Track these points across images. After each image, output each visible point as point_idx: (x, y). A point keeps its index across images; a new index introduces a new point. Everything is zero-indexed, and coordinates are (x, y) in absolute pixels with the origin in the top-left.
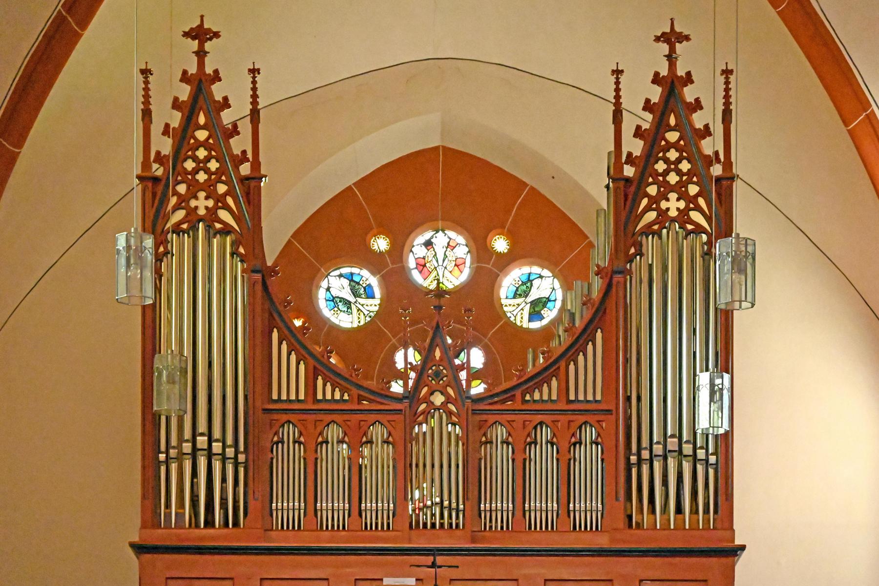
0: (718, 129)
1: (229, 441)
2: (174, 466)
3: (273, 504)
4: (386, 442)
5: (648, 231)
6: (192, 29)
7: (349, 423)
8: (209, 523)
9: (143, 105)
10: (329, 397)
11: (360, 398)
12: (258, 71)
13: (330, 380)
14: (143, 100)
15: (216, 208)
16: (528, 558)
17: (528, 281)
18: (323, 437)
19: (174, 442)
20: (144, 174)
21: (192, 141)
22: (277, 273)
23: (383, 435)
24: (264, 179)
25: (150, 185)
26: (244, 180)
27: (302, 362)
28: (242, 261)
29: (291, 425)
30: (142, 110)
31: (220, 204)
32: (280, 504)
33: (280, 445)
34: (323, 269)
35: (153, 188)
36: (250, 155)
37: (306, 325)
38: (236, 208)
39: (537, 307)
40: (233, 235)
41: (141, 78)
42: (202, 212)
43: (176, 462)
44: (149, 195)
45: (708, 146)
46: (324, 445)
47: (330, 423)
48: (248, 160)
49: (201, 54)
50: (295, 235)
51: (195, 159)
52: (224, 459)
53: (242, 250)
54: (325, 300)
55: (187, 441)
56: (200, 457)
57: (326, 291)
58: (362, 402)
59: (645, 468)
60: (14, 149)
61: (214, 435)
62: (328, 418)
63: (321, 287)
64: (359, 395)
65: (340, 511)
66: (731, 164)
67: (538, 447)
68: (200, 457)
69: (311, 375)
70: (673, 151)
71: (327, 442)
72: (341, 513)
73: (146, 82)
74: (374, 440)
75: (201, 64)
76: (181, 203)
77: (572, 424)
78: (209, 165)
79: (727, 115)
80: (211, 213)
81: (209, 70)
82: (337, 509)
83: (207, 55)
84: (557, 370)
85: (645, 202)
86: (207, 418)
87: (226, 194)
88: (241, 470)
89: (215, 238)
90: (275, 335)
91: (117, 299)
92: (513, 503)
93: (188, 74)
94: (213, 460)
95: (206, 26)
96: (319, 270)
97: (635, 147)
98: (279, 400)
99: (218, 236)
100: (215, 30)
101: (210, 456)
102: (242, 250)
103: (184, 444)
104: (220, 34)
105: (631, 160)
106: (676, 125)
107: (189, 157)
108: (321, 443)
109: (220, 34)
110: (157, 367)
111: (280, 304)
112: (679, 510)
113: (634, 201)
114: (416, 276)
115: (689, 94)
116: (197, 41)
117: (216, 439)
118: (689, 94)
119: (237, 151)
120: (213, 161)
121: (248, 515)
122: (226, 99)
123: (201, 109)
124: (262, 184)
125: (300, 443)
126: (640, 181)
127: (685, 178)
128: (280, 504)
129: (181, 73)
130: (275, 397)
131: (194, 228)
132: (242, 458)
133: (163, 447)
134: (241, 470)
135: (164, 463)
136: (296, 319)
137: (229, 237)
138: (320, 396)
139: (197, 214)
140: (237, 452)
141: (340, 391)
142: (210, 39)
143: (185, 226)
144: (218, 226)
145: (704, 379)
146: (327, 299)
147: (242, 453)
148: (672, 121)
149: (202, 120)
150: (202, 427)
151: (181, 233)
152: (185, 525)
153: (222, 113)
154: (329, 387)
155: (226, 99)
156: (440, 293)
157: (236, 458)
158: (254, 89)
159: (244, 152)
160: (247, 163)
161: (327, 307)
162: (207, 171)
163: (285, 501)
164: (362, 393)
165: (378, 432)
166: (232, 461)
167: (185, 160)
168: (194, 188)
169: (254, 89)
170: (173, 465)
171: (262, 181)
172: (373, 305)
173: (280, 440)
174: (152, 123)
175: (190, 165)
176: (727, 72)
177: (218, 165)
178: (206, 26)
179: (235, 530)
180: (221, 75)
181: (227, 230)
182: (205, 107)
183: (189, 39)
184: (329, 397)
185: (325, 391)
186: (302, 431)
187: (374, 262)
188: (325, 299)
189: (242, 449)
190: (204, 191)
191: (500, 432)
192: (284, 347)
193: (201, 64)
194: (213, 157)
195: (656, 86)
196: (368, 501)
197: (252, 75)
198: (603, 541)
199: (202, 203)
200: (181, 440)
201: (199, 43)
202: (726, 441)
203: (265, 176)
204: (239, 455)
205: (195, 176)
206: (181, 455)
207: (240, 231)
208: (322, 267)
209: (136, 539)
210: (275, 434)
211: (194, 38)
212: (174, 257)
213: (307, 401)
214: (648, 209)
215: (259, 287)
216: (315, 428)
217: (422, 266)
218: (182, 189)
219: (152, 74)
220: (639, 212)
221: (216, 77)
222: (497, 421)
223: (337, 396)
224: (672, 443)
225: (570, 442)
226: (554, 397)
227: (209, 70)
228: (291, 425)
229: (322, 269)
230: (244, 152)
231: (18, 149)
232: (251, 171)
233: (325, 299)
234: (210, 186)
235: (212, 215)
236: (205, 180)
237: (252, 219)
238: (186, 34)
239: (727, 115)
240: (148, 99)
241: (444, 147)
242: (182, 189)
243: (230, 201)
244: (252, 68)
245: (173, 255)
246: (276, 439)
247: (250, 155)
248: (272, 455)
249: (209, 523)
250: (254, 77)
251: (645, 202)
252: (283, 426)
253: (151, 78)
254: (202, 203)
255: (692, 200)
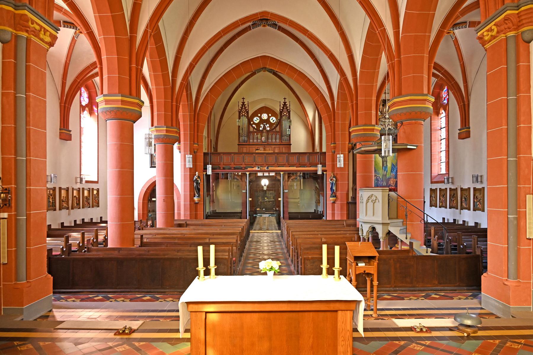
0: (289, 107)
5: (283, 116)
8: (244, 142)
17: (273, 118)
26: (247, 111)
39: (273, 121)
45: (288, 108)
49: (243, 100)
52: (246, 137)
79: (290, 106)
86: (1, 71)
97: (282, 108)
98: (477, 244)
105: (281, 109)
112: (286, 141)
113: (178, 251)
114: (263, 118)
115: (286, 104)
118: (286, 104)
126: (282, 112)
131: (243, 116)
145: (288, 129)
156: (265, 119)
165: (259, 134)
168: (243, 112)
172: (258, 121)
175: (242, 110)
176: (290, 102)
181: (246, 116)
185: (255, 130)
187: (259, 117)
191: (270, 134)
198: (279, 144)
199: (244, 114)
202: (290, 135)
217: (263, 117)
221: (245, 102)
224: (285, 135)
235: (244, 115)
239: (290, 106)
241: (265, 107)
249: (244, 142)
254: (244, 114)
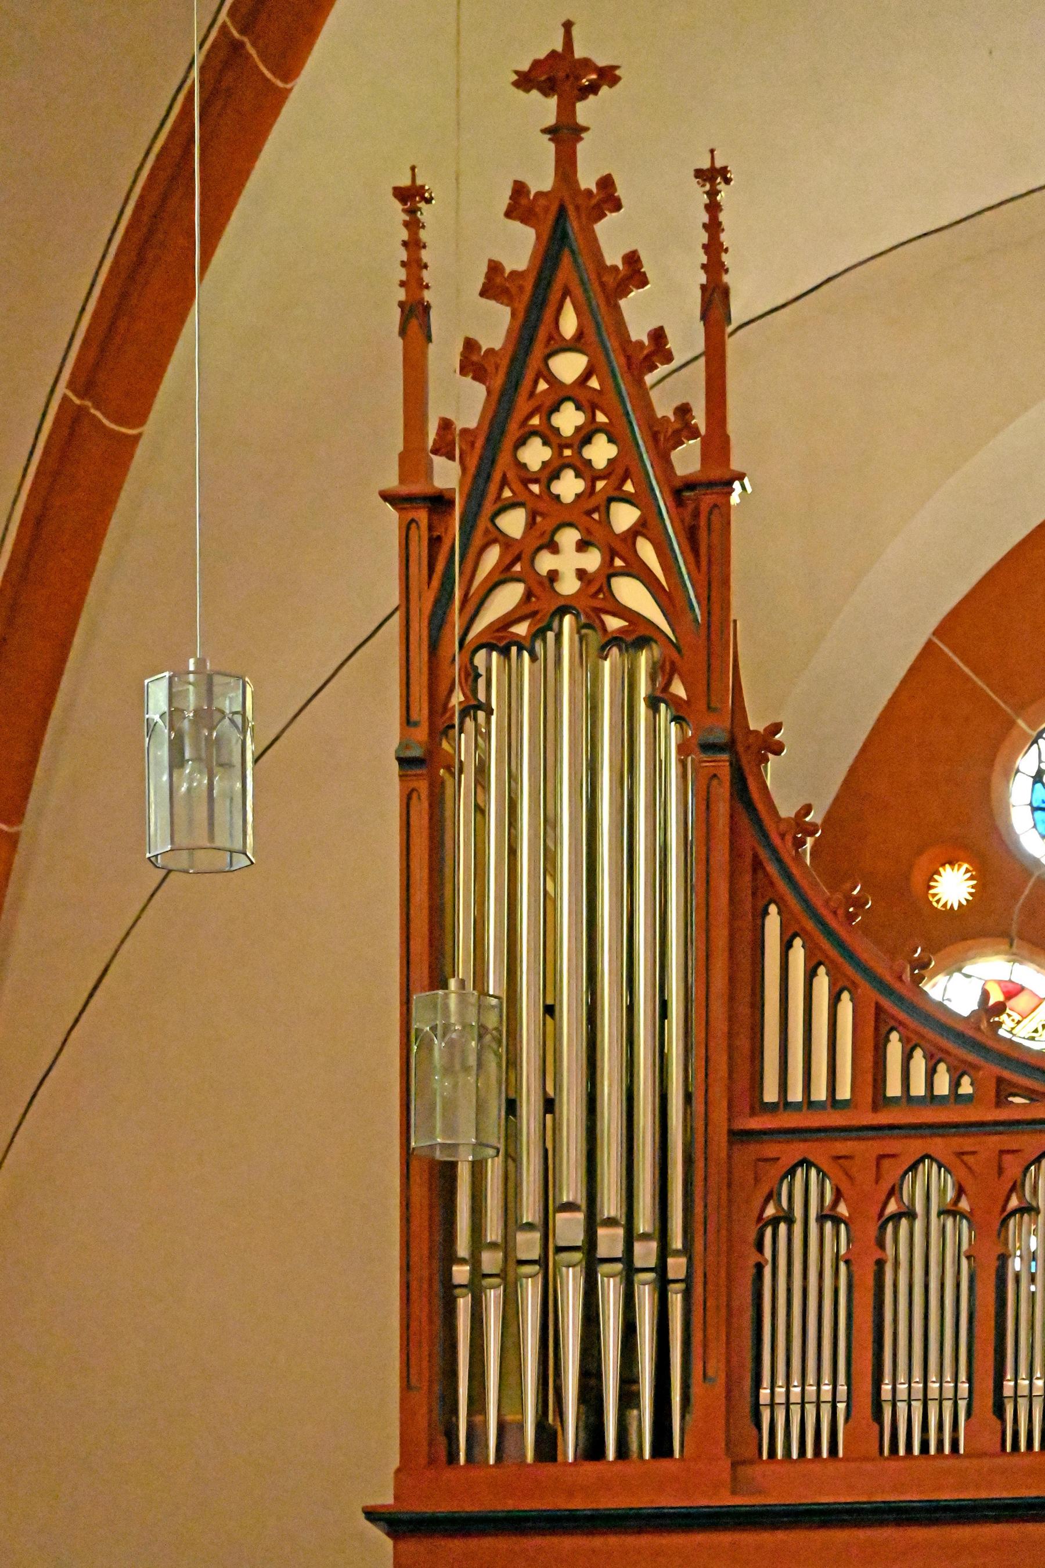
1: (644, 1223)
2: (493, 1299)
3: (762, 1391)
4: (950, 1212)
6: (536, 64)
7: (970, 1159)
9: (706, 272)
10: (918, 1089)
11: (1003, 1091)
12: (723, 172)
13: (922, 1043)
14: (704, 259)
15: (609, 573)
16: (488, 1543)
18: (1022, 1197)
19: (493, 1232)
20: (406, 490)
21: (542, 386)
22: (778, 749)
23: (942, 1192)
24: (737, 485)
25: (422, 516)
27: (846, 996)
28: (677, 719)
29: (813, 1172)
30: (703, 288)
31: (618, 562)
32: (780, 1391)
33: (783, 1228)
34: (1025, 720)
35: (430, 528)
36: (699, 419)
37: (855, 893)
38: (665, 575)
40: (654, 646)
41: (397, 210)
42: (568, 586)
43: (497, 1287)
44: (420, 549)
46: (904, 1222)
47: (921, 1160)
48: (694, 433)
50: (943, 630)
51: (550, 436)
53: (678, 689)
54: (1029, 808)
55: (530, 1226)
56: (564, 1269)
57: (1034, 783)
58: (1010, 1099)
59: (493, 1299)
60: (123, 430)
61: (602, 1206)
62: (915, 1147)
63: (1018, 771)
64: (1000, 1081)
65: (1034, 1399)
66: (726, 440)
67: (798, 1228)
68: (564, 1269)
69: (869, 1031)
70: (569, 408)
71: (911, 1215)
72: (948, 1405)
73: (413, 224)
74: (919, 1208)
75: (566, 164)
76: (513, 563)
77: (886, 1163)
78: (588, 452)
80: (593, 589)
81: (587, 180)
82: (799, 1401)
83: (583, 135)
84: (883, 1016)
85: (492, 556)
87: (634, 532)
88: (676, 1302)
89: (605, 659)
90: (773, 923)
91: (149, 858)
92: (970, 1380)
93: (529, 192)
94: (599, 1276)
95: (579, 53)
96: (1011, 724)
98: (931, 1098)
99: (615, 651)
100: (601, 62)
101: (592, 1264)
102: (678, 689)
103: (521, 1237)
104: (618, 72)
106: (580, 335)
107: (534, 432)
108: (896, 1217)
109: (618, 72)
110: (417, 1029)
111: (783, 836)
116: (556, 97)
117: (609, 1218)
119: (664, 408)
120: (601, 439)
121: (850, 1420)
122: (632, 259)
123: (566, 292)
124: (735, 499)
125: (837, 1220)
127: (600, 485)
128: (780, 1391)
129: (509, 193)
130: (771, 1095)
132: (677, 1266)
133: (463, 1249)
134: (676, 1302)
135: (464, 1291)
136: (947, 866)
137: (644, 651)
138: (894, 1089)
139: (556, 592)
140: (664, 1252)
141: (948, 1070)
142: (593, 89)
143: (521, 629)
144: (614, 623)
146: (1035, 805)
147: (677, 1253)
148: (569, 324)
149: (569, 324)
150: (572, 1189)
151: (514, 650)
152: (524, 1455)
153: (623, 303)
154: (919, 1064)
155: (632, 259)
157: (661, 1268)
158: (713, 227)
159: (684, 411)
160: (691, 442)
161: (1035, 826)
162: (583, 469)
163: (796, 1381)
164: (1006, 1074)
166: (651, 1276)
167: (522, 442)
169: (713, 227)
170: (492, 1294)
171: (733, 490)
173: (904, 1210)
174: (429, 338)
177: (612, 451)
178: (579, 53)
179: (621, 1466)
180: (620, 192)
182: (578, 291)
183: (535, 93)
184: (918, 1089)
186: (842, 1188)
188: (1031, 804)
189: (677, 1243)
190: (571, 525)
192: (798, 954)
193: (566, 164)
194: (600, 429)
195: (517, 225)
196: (1023, 1373)
197: (708, 187)
200: (511, 1221)
201: (558, 106)
203: (740, 477)
204: (670, 1261)
205: (549, 488)
206: (512, 1262)
207: (676, 638)
208: (1019, 715)
209: (386, 1498)
210: (891, 1193)
211: (548, 88)
212: (494, 718)
213: (856, 1107)
214: (502, 577)
215: (723, 791)
216: (757, 1180)
218: (513, 523)
219: (428, 201)
220: (664, 583)
222: (928, 1156)
223: (942, 1085)
225: (760, 1218)
226: (844, 1092)
227: (587, 180)
228: (813, 1172)
229: (1021, 723)
230: (684, 411)
231: (133, 427)
232: (702, 464)
233: (1031, 804)
234: (589, 513)
236: (578, 496)
237: (707, 602)
238: (525, 81)
240: (719, 257)
242: (513, 523)
243: (646, 551)
244: (706, 165)
245: (489, 712)
246: (770, 1211)
247: (699, 419)
248: (880, 1252)
250: (713, 194)
251: (492, 556)
252: (792, 1172)
253: (426, 214)
255: (619, 546)
